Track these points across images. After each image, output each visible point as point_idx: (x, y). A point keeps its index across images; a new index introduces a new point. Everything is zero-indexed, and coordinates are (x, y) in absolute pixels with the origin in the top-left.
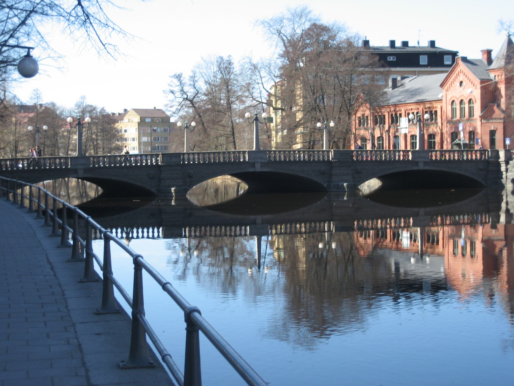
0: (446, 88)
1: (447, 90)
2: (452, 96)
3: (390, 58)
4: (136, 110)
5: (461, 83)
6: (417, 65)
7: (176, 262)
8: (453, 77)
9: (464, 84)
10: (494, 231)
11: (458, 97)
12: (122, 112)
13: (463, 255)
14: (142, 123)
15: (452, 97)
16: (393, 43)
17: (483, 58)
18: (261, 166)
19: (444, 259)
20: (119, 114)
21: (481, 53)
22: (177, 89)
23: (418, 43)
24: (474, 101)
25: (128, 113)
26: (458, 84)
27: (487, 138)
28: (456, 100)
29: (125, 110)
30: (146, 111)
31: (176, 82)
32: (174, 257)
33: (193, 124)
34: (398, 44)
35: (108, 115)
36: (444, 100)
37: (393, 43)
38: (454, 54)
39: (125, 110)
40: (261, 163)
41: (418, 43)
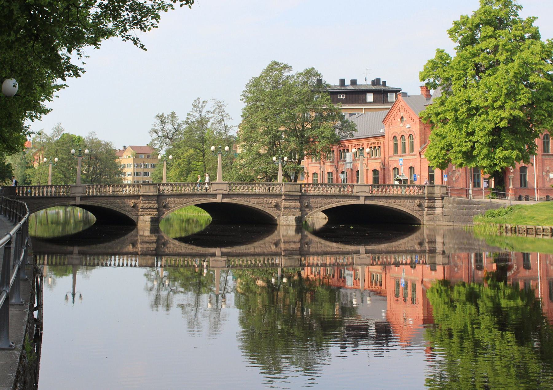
0: (388, 123)
1: (389, 126)
2: (393, 131)
3: (340, 96)
4: (131, 147)
5: (402, 118)
6: (364, 102)
7: (151, 289)
8: (395, 113)
9: (405, 119)
10: (433, 272)
11: (399, 133)
12: (122, 148)
13: (405, 300)
14: (137, 157)
15: (394, 133)
16: (342, 81)
17: (422, 94)
18: (223, 198)
19: (386, 303)
20: (120, 150)
21: (420, 89)
22: (158, 128)
23: (57, 97)
24: (414, 137)
25: (127, 150)
26: (399, 120)
27: (426, 174)
28: (397, 136)
29: (125, 147)
30: (141, 148)
31: (158, 122)
32: (150, 285)
33: (87, 151)
34: (347, 83)
35: (111, 150)
36: (386, 136)
37: (342, 81)
38: (397, 91)
39: (125, 147)
40: (223, 194)
41: (57, 97)
